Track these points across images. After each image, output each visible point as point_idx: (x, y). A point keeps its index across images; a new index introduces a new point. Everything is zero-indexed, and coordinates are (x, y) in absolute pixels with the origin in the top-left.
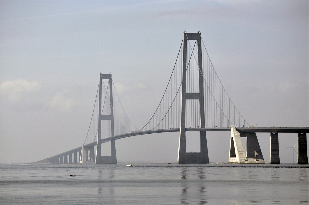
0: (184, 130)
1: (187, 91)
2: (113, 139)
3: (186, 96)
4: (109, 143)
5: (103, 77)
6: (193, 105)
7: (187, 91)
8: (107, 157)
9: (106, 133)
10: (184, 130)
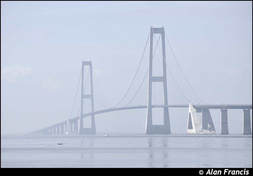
0: (151, 107)
1: (153, 75)
2: (93, 114)
3: (153, 79)
4: (90, 117)
5: (84, 63)
6: (158, 86)
7: (153, 75)
8: (87, 129)
9: (88, 110)
10: (151, 107)
